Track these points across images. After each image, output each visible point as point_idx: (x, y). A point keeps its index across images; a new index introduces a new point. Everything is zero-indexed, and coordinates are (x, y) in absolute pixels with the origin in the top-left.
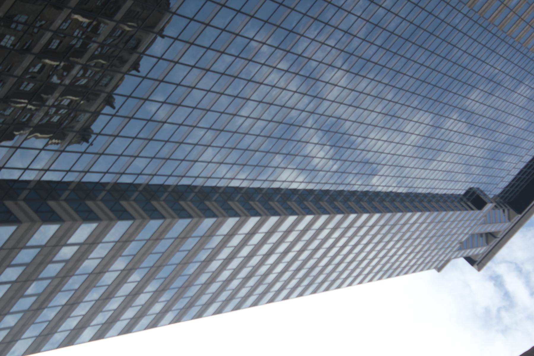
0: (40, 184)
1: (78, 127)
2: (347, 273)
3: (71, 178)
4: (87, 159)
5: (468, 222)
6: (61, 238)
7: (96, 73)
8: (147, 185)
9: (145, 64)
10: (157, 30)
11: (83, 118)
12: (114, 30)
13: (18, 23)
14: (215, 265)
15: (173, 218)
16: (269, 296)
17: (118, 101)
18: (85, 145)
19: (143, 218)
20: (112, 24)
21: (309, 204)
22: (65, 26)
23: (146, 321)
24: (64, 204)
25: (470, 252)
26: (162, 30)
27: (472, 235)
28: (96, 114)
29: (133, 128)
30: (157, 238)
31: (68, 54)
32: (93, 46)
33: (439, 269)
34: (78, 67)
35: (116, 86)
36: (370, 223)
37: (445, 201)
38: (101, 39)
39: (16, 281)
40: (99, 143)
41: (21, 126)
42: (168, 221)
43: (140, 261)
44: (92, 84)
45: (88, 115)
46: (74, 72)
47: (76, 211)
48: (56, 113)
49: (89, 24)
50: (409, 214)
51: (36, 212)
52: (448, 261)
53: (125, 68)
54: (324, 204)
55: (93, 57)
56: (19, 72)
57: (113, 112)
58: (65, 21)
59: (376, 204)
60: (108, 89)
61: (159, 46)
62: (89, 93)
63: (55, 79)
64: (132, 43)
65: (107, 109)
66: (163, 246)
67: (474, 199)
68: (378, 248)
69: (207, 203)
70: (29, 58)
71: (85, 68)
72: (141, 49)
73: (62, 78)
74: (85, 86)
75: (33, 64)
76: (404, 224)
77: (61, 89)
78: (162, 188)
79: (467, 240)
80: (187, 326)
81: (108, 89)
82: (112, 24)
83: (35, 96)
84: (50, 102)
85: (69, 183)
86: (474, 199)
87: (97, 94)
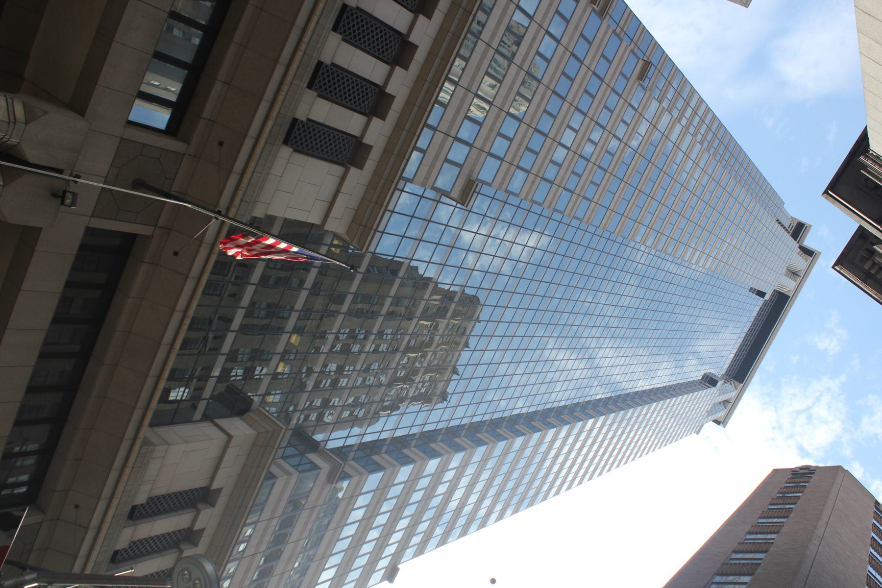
0: (471, 425)
1: (438, 392)
2: (636, 449)
3: (441, 426)
4: (448, 412)
5: (711, 396)
6: (489, 454)
7: (442, 355)
8: (393, 438)
9: (472, 342)
10: (475, 318)
11: (440, 386)
12: (448, 325)
13: (387, 334)
14: (547, 463)
15: (473, 447)
16: (541, 496)
17: (460, 369)
18: (445, 403)
19: (494, 442)
20: (446, 321)
21: (565, 417)
22: (416, 330)
23: (526, 502)
24: (441, 444)
25: (715, 417)
26: (478, 317)
27: (714, 405)
28: (449, 381)
29: (474, 384)
30: (505, 453)
31: (422, 347)
32: (437, 338)
33: (698, 433)
34: (430, 354)
35: (457, 360)
36: (644, 412)
37: (690, 386)
38: (440, 332)
39: (421, 500)
40: (454, 400)
41: (402, 400)
42: (528, 436)
43: (498, 470)
44: (441, 362)
45: (443, 383)
46: (428, 358)
47: (449, 447)
48: (423, 386)
49: (431, 325)
50: (668, 400)
51: (424, 453)
52: (702, 426)
53: (460, 348)
54: (589, 411)
55: (438, 346)
56: (393, 365)
57: (458, 377)
58: (416, 326)
59: (644, 398)
60: (453, 363)
61: (479, 328)
62: (439, 369)
63: (417, 365)
64: (461, 330)
65: (455, 377)
66: (510, 458)
67: (710, 381)
68: (639, 432)
69: (533, 423)
70: (398, 355)
71: (435, 353)
72: (467, 333)
73: (421, 363)
74: (437, 365)
75: (401, 359)
76: (653, 412)
77: (422, 370)
78: (502, 419)
79: (711, 408)
80: (526, 514)
81: (453, 363)
82: (446, 321)
83: (408, 379)
84: (417, 380)
85: (440, 430)
86: (710, 381)
87: (446, 369)
